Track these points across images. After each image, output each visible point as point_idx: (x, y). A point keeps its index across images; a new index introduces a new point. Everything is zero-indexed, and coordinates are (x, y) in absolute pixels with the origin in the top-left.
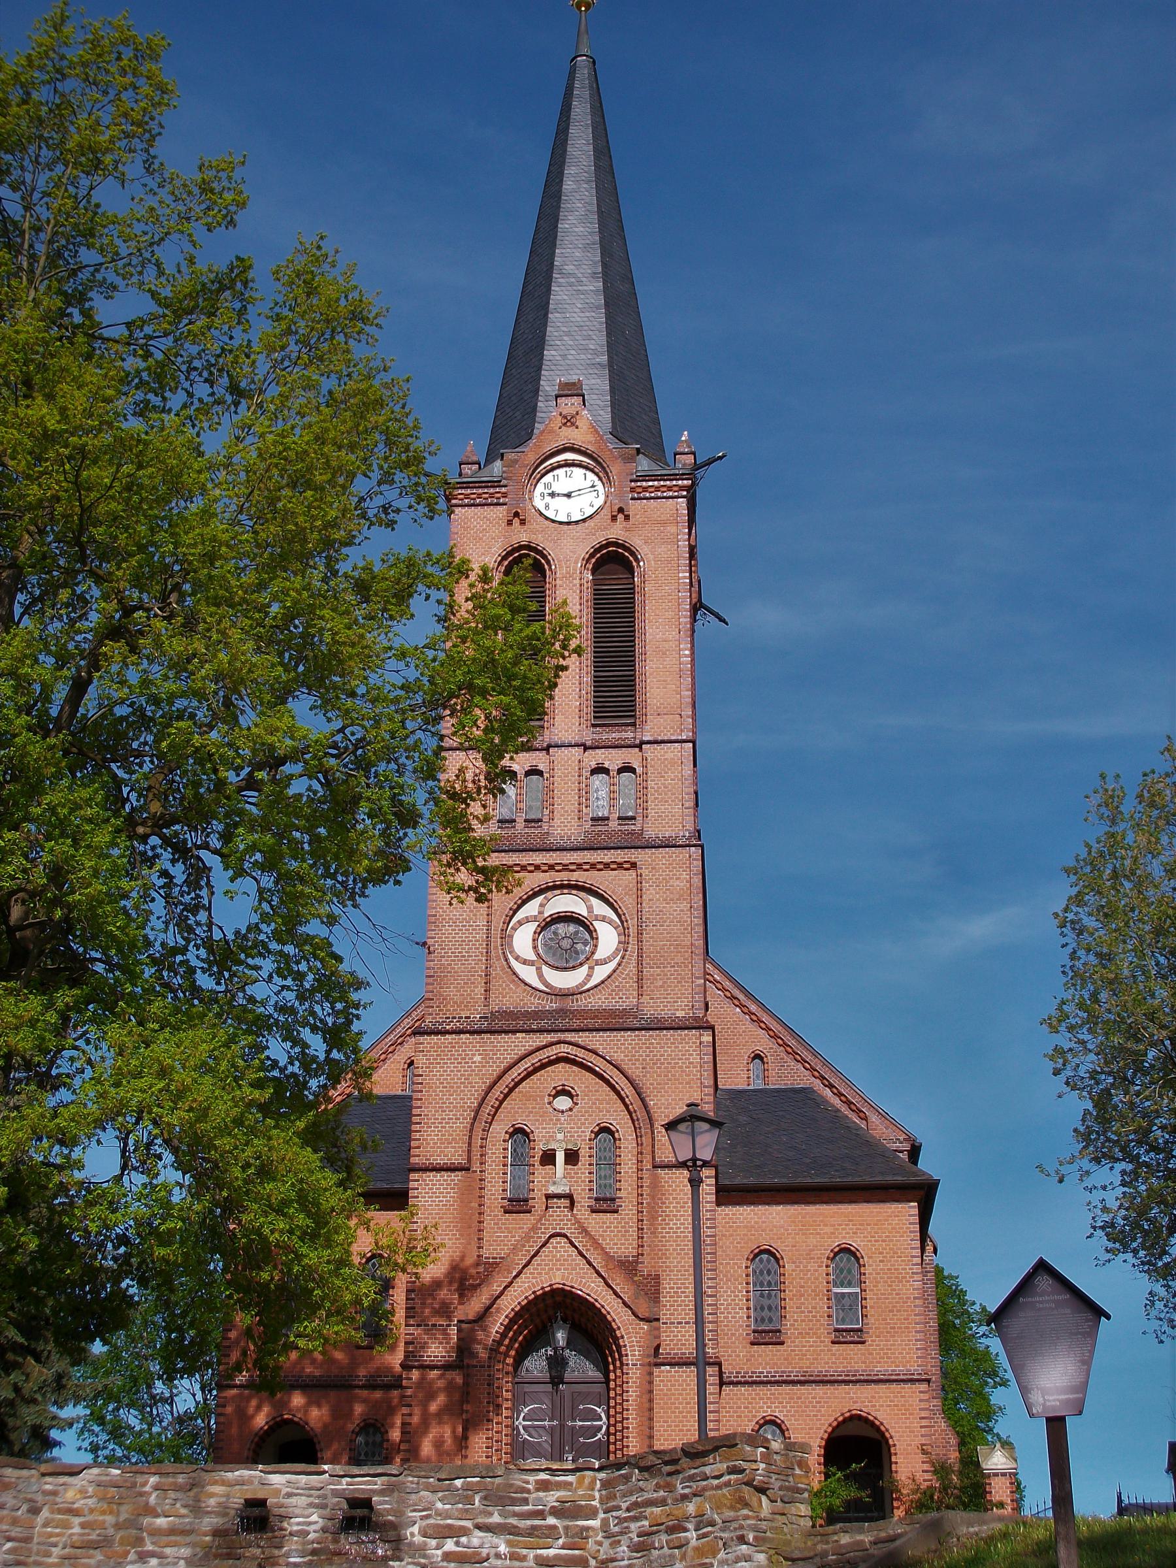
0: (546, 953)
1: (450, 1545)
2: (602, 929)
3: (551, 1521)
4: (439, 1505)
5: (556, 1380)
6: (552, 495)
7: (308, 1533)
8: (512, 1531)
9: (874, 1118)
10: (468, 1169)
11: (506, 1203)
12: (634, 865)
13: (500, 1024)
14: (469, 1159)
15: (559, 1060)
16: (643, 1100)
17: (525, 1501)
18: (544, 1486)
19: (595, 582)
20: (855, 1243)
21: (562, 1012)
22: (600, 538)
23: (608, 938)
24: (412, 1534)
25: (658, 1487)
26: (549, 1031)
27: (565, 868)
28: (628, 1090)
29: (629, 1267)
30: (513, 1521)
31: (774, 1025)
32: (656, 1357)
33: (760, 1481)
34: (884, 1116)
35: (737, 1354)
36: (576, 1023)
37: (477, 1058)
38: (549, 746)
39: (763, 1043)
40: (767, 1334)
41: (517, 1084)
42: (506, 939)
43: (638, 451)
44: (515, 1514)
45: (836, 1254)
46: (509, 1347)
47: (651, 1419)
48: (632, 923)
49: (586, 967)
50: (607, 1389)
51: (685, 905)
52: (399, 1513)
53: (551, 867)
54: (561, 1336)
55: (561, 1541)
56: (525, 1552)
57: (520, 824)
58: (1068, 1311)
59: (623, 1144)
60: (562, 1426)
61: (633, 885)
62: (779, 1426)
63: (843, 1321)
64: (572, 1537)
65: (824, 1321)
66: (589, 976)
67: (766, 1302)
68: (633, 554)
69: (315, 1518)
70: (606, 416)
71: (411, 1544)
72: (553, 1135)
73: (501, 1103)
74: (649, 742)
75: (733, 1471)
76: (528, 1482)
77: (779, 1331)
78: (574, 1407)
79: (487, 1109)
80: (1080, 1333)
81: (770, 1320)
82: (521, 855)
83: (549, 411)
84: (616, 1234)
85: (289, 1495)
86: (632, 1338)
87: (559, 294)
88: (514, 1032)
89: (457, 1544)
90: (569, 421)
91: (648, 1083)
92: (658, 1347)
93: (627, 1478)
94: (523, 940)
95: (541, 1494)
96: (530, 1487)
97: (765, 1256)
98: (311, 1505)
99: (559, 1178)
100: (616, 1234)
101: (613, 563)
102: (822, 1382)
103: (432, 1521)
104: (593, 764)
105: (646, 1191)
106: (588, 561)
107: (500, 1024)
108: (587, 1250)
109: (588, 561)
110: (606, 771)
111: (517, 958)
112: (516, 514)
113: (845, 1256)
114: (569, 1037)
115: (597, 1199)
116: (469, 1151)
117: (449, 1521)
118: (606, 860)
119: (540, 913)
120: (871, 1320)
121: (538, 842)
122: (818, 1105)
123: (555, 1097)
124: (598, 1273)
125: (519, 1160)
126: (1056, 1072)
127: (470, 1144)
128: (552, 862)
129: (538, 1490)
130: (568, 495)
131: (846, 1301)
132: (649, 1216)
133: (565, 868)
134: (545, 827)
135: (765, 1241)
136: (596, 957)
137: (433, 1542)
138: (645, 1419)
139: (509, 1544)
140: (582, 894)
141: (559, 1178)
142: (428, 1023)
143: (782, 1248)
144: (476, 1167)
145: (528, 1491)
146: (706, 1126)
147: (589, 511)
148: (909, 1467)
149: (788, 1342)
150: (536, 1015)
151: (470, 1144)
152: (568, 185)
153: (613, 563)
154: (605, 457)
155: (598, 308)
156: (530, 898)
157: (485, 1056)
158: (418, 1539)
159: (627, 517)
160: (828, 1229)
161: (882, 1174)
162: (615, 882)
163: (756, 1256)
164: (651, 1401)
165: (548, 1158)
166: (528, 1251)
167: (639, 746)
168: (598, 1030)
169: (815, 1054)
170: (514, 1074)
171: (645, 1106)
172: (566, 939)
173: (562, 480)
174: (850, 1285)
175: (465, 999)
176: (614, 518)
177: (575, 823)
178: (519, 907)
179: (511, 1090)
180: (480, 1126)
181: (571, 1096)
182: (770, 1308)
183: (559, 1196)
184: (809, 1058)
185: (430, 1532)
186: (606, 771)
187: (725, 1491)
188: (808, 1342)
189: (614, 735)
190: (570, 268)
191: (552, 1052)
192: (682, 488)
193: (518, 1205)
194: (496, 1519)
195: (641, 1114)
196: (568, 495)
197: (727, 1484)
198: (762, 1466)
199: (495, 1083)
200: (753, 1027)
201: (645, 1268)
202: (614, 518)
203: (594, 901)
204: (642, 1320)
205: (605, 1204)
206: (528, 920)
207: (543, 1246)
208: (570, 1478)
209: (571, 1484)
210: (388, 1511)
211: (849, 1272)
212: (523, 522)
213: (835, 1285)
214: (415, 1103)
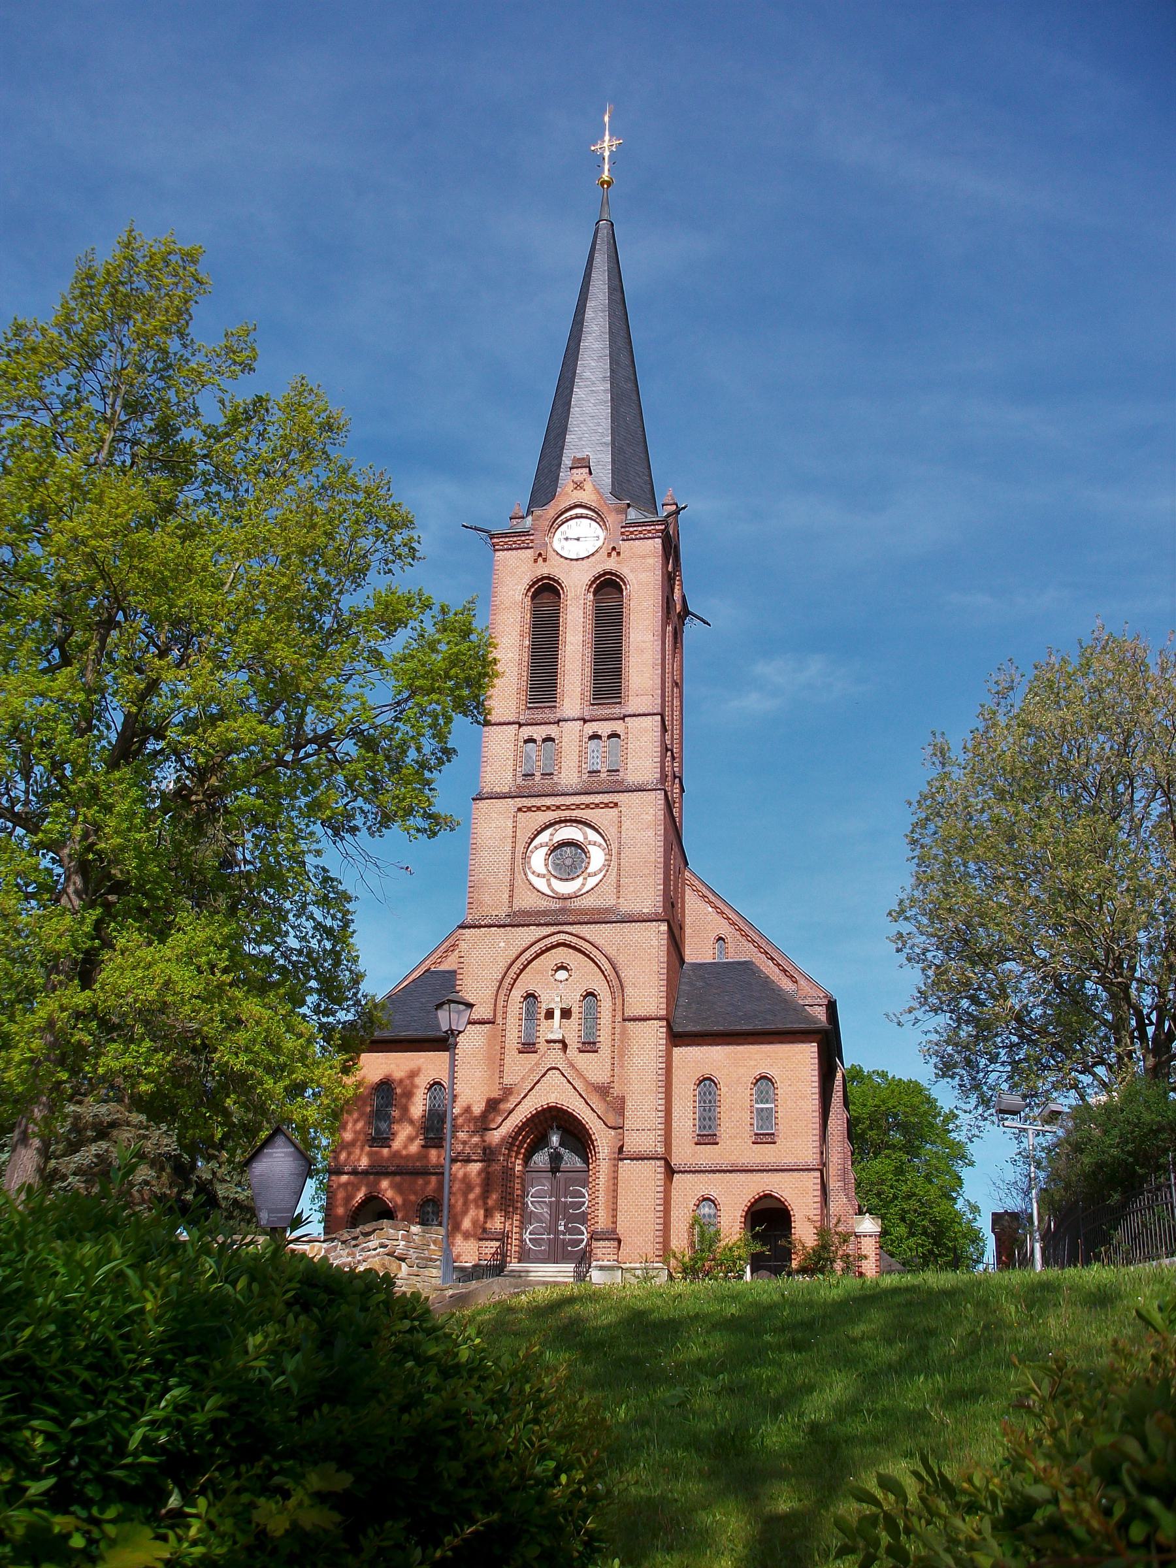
0: (555, 870)
5: (555, 1170)
6: (567, 539)
9: (802, 982)
11: (520, 1046)
12: (616, 804)
13: (518, 920)
15: (559, 945)
16: (617, 973)
19: (596, 601)
20: (771, 1072)
21: (563, 910)
22: (599, 569)
23: (597, 857)
25: (349, 1254)
26: (552, 925)
27: (568, 808)
28: (606, 966)
29: (603, 1091)
31: (732, 916)
32: (620, 1154)
34: (809, 980)
35: (684, 1152)
36: (571, 919)
37: (502, 944)
38: (559, 721)
39: (725, 929)
40: (707, 1137)
41: (529, 962)
42: (526, 858)
43: (629, 505)
45: (758, 1081)
46: (520, 1147)
47: (616, 1197)
48: (614, 847)
49: (581, 878)
50: (584, 1178)
51: (651, 833)
53: (558, 807)
54: (555, 1139)
57: (537, 778)
59: (603, 1004)
60: (558, 1201)
61: (616, 819)
62: (713, 1202)
63: (762, 1128)
65: (748, 1128)
66: (583, 885)
68: (622, 580)
70: (608, 480)
72: (551, 999)
73: (518, 976)
74: (630, 716)
75: (383, 1246)
78: (567, 1188)
79: (508, 980)
81: (710, 1127)
82: (537, 799)
83: (567, 477)
84: (595, 1068)
87: (579, 393)
88: (528, 925)
90: (579, 486)
91: (620, 961)
92: (621, 1147)
93: (336, 1247)
94: (538, 859)
97: (707, 1082)
99: (555, 1029)
100: (595, 1068)
101: (608, 586)
102: (702, 1171)
105: (617, 1037)
106: (590, 586)
107: (518, 920)
109: (590, 586)
110: (534, 741)
111: (533, 873)
112: (540, 555)
113: (764, 1082)
115: (584, 1043)
116: (495, 1010)
118: (597, 801)
120: (781, 1127)
121: (549, 790)
122: (754, 973)
123: (556, 971)
125: (531, 1016)
126: (899, 950)
127: (495, 1005)
128: (558, 804)
130: (578, 539)
131: (765, 1114)
132: (620, 1053)
133: (568, 808)
134: (555, 778)
135: (707, 1072)
136: (589, 871)
140: (580, 826)
141: (555, 1029)
142: (469, 921)
143: (718, 1076)
144: (499, 1020)
148: (804, 1233)
150: (545, 913)
151: (495, 1005)
152: (589, 314)
153: (608, 586)
154: (604, 510)
155: (606, 402)
156: (543, 830)
157: (507, 943)
159: (619, 554)
160: (752, 1063)
161: (791, 1022)
163: (701, 1082)
164: (616, 1184)
165: (550, 1015)
167: (623, 719)
168: (586, 923)
169: (761, 936)
170: (527, 955)
171: (618, 977)
172: (568, 857)
173: (575, 528)
174: (767, 1102)
175: (495, 903)
176: (609, 555)
177: (576, 775)
178: (536, 836)
179: (525, 967)
180: (503, 992)
181: (567, 970)
182: (710, 1119)
183: (555, 1041)
184: (757, 939)
186: (534, 741)
188: (735, 1142)
189: (539, 716)
190: (587, 374)
192: (658, 531)
193: (528, 1047)
195: (615, 982)
196: (578, 539)
197: (378, 1255)
199: (514, 962)
200: (718, 918)
201: (615, 1092)
202: (609, 555)
203: (589, 831)
205: (589, 1046)
211: (767, 1093)
212: (545, 560)
213: (757, 1102)
214: (459, 977)
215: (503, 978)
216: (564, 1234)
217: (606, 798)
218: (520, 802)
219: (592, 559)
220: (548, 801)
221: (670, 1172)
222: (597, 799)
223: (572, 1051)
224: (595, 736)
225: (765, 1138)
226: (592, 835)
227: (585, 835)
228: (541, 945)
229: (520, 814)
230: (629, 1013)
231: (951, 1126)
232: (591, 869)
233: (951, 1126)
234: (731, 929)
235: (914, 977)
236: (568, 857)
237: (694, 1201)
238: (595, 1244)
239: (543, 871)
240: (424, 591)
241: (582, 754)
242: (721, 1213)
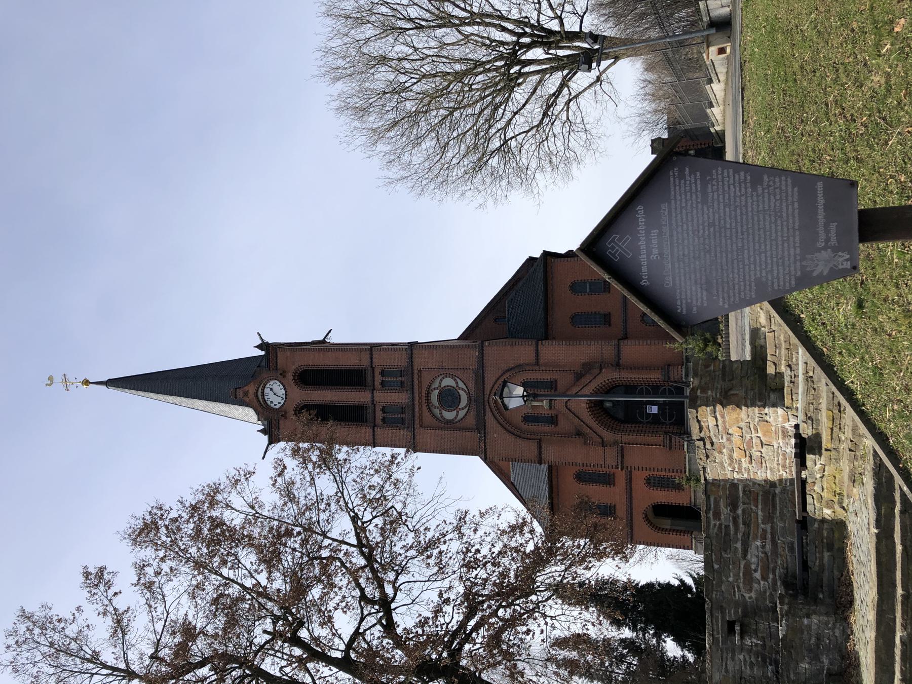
1: (758, 575)
2: (444, 384)
3: (739, 511)
4: (731, 579)
7: (751, 662)
8: (746, 536)
10: (540, 440)
17: (727, 527)
18: (717, 515)
22: (292, 382)
23: (448, 382)
24: (750, 598)
30: (740, 535)
32: (618, 365)
33: (721, 395)
44: (736, 533)
52: (737, 604)
55: (754, 508)
56: (760, 530)
58: (664, 206)
64: (750, 500)
66: (463, 389)
69: (741, 657)
71: (757, 599)
76: (715, 525)
80: (704, 188)
85: (727, 671)
86: (609, 376)
88: (485, 420)
89: (756, 571)
94: (449, 415)
95: (722, 517)
96: (718, 523)
98: (733, 659)
103: (741, 585)
114: (486, 399)
117: (741, 575)
129: (720, 519)
130: (86, 382)
133: (420, 398)
137: (756, 585)
139: (755, 538)
144: (539, 437)
145: (720, 525)
146: (506, 390)
147: (282, 387)
158: (753, 595)
162: (426, 378)
185: (748, 587)
187: (727, 418)
189: (369, 379)
194: (739, 545)
198: (710, 393)
204: (601, 371)
206: (457, 383)
208: (712, 499)
209: (715, 499)
210: (736, 612)
217: (416, 377)
220: (417, 409)
221: (625, 337)
222: (416, 382)
226: (436, 384)
230: (533, 360)
235: (517, 196)
236: (449, 398)
238: (672, 379)
240: (28, 610)
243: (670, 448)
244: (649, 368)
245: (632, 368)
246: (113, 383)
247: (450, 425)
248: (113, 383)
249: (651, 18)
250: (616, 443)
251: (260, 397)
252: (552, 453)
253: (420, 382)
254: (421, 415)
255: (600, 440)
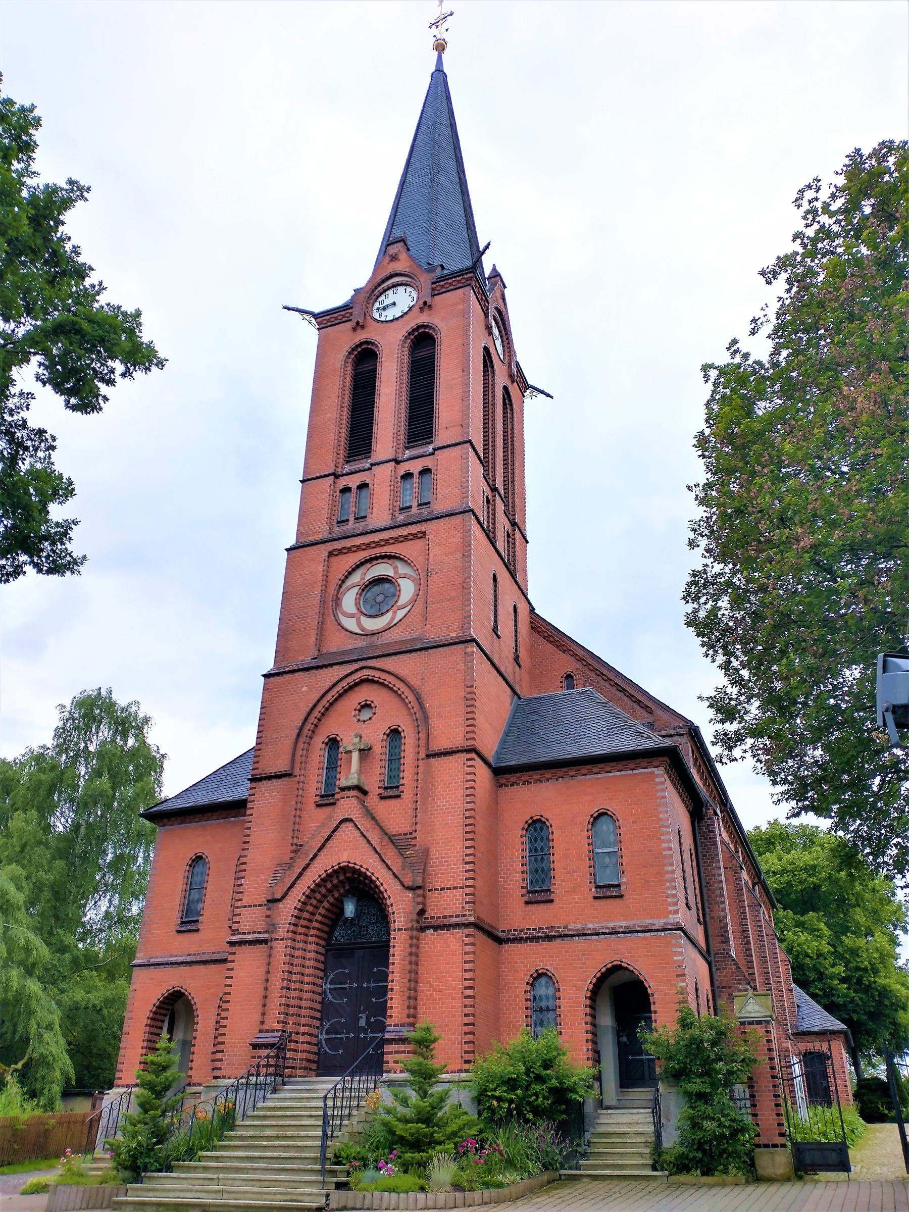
14: (293, 767)
22: (413, 324)
23: (407, 590)
32: (423, 922)
42: (337, 601)
67: (295, 840)
77: (549, 890)
84: (395, 815)
86: (400, 907)
91: (425, 690)
94: (349, 602)
101: (422, 342)
104: (402, 473)
108: (367, 831)
114: (370, 663)
119: (363, 579)
124: (375, 849)
130: (440, 47)
133: (378, 544)
136: (399, 604)
138: (406, 980)
140: (390, 562)
144: (297, 772)
149: (557, 900)
153: (422, 342)
166: (323, 836)
183: (349, 788)
188: (573, 902)
191: (357, 677)
193: (327, 800)
199: (315, 706)
203: (399, 564)
204: (409, 888)
207: (362, 833)
215: (303, 724)
216: (365, 1031)
217: (413, 529)
218: (330, 547)
219: (406, 318)
222: (404, 531)
223: (372, 800)
224: (408, 476)
225: (608, 892)
226: (402, 569)
227: (395, 568)
228: (344, 684)
229: (333, 559)
230: (436, 746)
231: (711, 652)
232: (401, 602)
233: (711, 652)
234: (579, 665)
237: (527, 978)
239: (353, 610)
241: (395, 494)
242: (561, 994)
243: (255, 1046)
244: (413, 999)
245: (414, 957)
246: (439, 79)
247: (331, 603)
248: (439, 79)
249: (650, 1110)
250: (272, 927)
251: (385, 285)
252: (267, 801)
253: (406, 538)
254: (349, 550)
255: (278, 896)
